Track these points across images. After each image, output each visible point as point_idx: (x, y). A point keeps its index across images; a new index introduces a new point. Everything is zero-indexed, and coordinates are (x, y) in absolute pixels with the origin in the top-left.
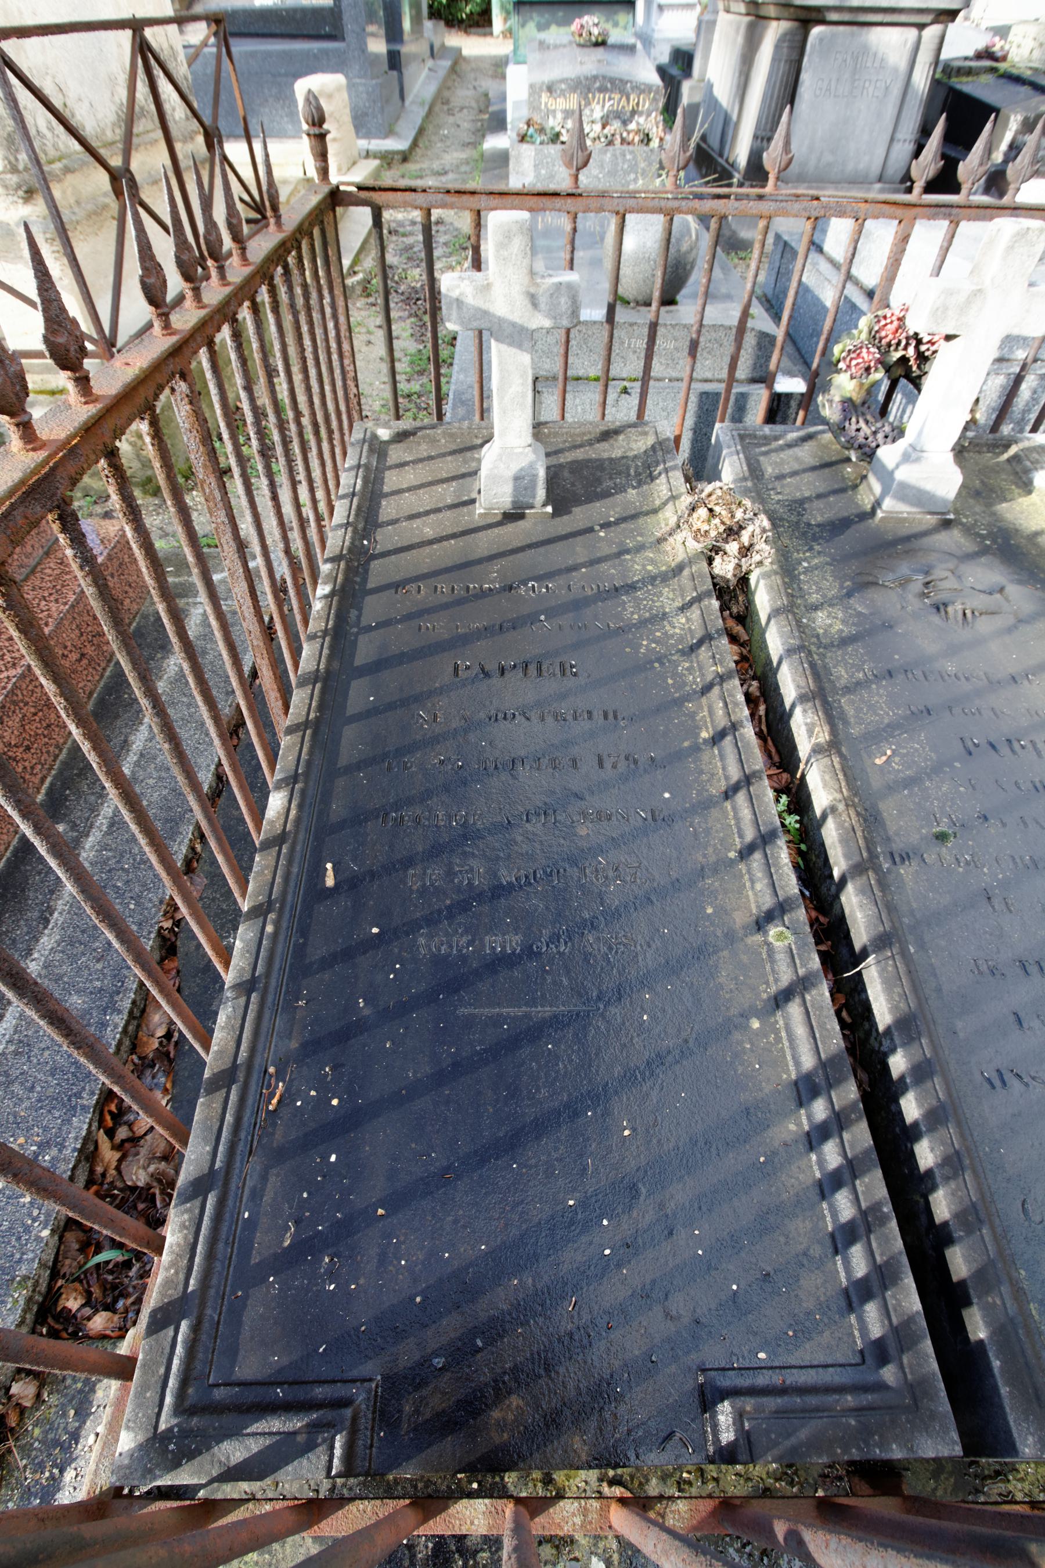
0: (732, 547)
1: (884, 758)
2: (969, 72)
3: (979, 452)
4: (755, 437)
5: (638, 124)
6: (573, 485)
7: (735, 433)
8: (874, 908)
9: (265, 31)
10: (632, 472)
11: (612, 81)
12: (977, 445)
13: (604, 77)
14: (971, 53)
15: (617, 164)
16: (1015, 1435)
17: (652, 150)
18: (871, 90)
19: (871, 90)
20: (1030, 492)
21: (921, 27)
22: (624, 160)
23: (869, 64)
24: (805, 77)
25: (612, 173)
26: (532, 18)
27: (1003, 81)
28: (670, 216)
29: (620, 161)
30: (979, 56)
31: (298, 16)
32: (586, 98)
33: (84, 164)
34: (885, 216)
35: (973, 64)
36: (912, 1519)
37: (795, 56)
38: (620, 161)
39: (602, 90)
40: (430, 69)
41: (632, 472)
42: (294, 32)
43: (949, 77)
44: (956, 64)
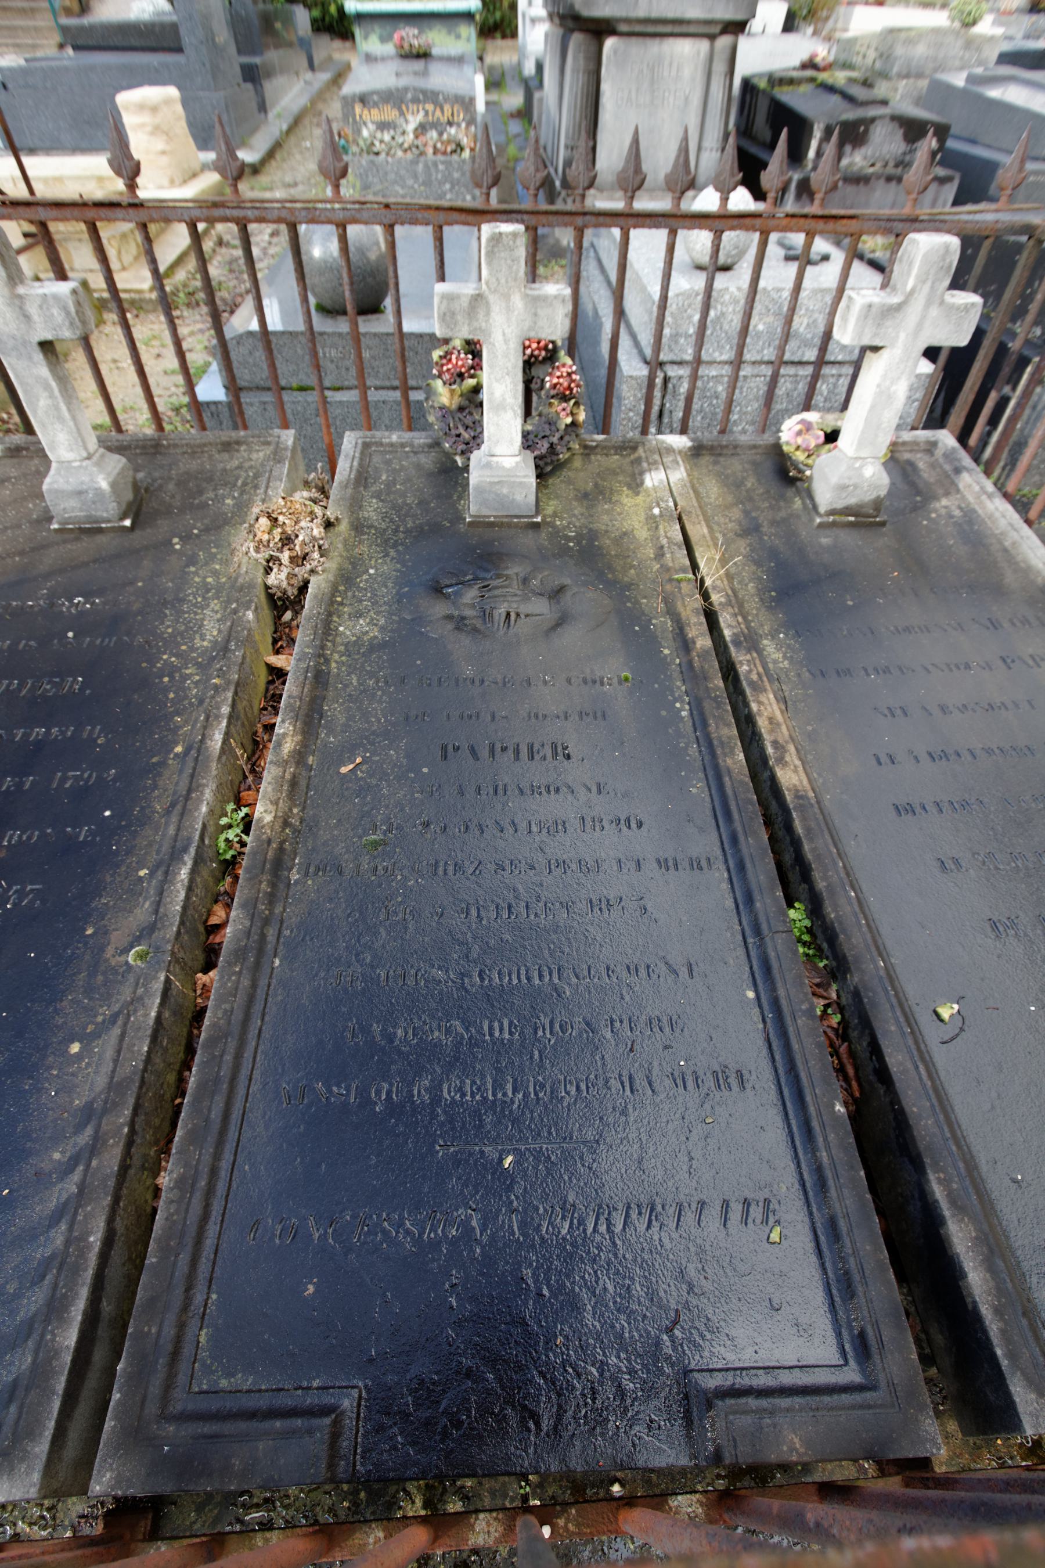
0: (285, 556)
1: (351, 766)
2: (791, 82)
3: (607, 455)
4: (381, 444)
5: (449, 134)
6: (173, 497)
7: (360, 441)
8: (248, 923)
9: (125, 44)
10: (240, 483)
11: (424, 92)
12: (605, 448)
13: (415, 89)
14: (797, 63)
15: (430, 175)
16: (95, 1472)
17: (464, 161)
18: (671, 100)
19: (671, 100)
20: (637, 494)
21: (712, 37)
22: (437, 171)
23: (666, 74)
24: (605, 87)
25: (427, 183)
26: (373, 30)
27: (819, 91)
28: (342, 227)
29: (433, 170)
30: (804, 66)
31: (157, 29)
32: (400, 109)
33: (39, 179)
34: (457, 223)
35: (795, 74)
36: (911, 1492)
37: (592, 66)
38: (433, 170)
39: (416, 101)
40: (306, 82)
41: (240, 483)
42: (154, 45)
43: (773, 87)
44: (777, 75)
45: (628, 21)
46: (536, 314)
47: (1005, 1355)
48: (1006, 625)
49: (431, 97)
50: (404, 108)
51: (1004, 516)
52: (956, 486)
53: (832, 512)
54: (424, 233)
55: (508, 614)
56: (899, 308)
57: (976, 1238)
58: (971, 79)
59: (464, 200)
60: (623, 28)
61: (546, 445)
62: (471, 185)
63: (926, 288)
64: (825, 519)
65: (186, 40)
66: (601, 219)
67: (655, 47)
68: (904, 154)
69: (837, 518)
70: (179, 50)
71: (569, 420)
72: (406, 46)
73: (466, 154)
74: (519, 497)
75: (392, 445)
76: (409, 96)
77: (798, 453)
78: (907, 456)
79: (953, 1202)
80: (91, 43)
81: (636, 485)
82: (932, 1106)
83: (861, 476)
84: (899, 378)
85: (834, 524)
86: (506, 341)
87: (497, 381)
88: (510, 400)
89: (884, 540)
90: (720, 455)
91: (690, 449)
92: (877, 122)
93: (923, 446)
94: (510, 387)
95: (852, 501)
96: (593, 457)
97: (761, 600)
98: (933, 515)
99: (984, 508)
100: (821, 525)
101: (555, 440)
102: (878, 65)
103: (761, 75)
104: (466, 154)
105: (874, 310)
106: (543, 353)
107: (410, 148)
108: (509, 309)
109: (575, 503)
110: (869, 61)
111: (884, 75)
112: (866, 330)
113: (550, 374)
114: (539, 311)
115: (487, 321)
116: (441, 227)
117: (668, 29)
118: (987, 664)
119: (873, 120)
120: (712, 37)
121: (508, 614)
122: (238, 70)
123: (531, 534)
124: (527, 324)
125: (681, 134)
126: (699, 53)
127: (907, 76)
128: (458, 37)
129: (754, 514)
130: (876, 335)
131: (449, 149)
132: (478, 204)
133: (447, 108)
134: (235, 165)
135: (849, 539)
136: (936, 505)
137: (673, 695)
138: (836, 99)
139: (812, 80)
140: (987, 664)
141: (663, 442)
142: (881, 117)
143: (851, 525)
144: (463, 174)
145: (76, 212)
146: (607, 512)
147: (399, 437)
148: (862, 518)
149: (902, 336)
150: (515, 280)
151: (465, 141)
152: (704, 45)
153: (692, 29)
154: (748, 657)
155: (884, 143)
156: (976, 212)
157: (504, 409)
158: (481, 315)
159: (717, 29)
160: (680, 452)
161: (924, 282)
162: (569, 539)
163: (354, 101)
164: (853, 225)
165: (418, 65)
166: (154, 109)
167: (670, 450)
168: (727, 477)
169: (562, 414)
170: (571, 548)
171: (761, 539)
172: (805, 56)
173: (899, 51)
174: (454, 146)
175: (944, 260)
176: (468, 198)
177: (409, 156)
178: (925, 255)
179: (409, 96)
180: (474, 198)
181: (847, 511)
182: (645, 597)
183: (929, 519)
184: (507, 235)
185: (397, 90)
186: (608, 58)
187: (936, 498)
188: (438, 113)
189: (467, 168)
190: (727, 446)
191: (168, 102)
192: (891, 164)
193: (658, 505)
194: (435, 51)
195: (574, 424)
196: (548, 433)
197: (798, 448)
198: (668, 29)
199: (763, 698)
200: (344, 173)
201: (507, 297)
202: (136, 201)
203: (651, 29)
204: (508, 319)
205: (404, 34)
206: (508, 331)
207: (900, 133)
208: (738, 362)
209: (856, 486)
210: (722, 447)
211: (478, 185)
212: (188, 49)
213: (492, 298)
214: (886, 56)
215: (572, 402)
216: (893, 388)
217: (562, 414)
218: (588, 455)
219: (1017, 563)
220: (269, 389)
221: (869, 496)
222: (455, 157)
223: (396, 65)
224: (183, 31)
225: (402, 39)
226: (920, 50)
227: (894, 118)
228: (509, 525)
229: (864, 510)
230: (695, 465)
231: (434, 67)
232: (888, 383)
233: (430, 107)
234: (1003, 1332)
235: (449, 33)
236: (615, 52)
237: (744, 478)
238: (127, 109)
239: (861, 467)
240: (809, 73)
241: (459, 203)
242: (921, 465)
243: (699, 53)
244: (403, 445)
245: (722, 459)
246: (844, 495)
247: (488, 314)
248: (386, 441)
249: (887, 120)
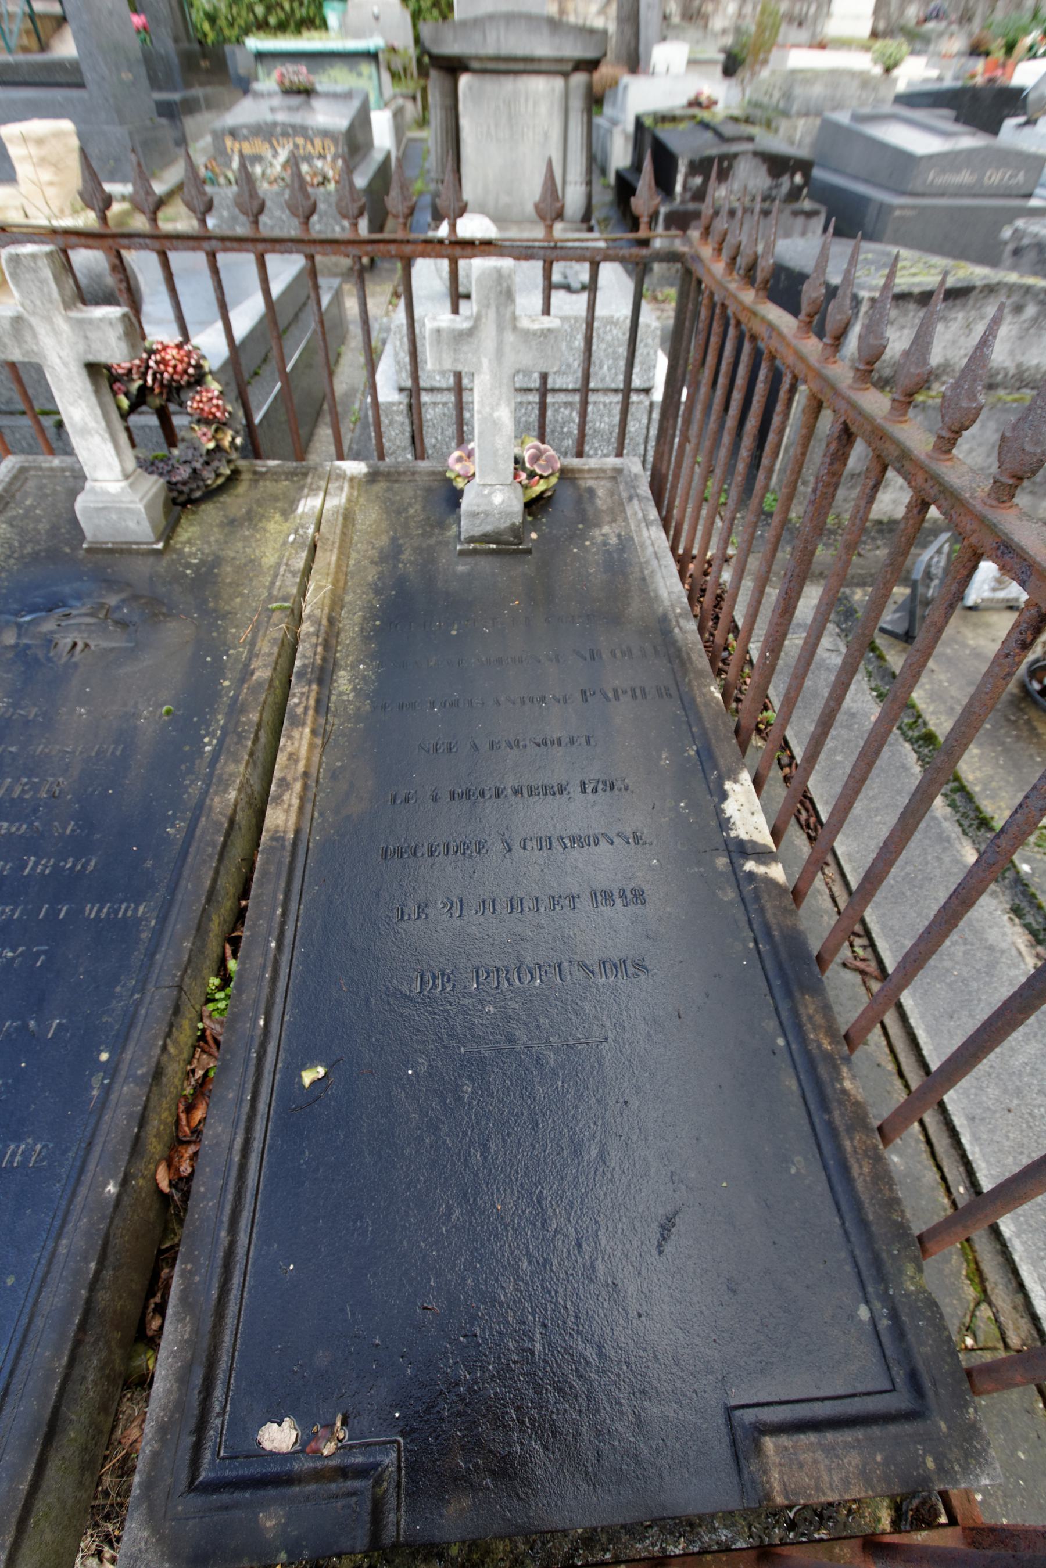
3: (276, 481)
4: (41, 469)
11: (293, 127)
12: (275, 473)
14: (683, 101)
17: (329, 193)
24: (464, 122)
35: (678, 112)
37: (449, 102)
39: (285, 134)
45: (479, 58)
46: (86, 338)
47: (140, 1484)
48: (606, 656)
49: (302, 131)
50: (275, 142)
51: (653, 545)
52: (624, 511)
53: (471, 540)
54: (248, 259)
55: (75, 645)
56: (471, 332)
57: (186, 1341)
58: (857, 118)
59: (333, 231)
60: (475, 65)
61: (189, 470)
62: (338, 217)
63: (492, 314)
64: (466, 546)
65: (88, 76)
66: (228, 244)
67: (509, 84)
68: (771, 188)
69: (478, 546)
70: (81, 85)
71: (211, 445)
72: (287, 83)
73: (331, 187)
74: (132, 525)
75: (52, 469)
76: (279, 130)
77: (459, 480)
78: (591, 483)
79: (184, 1299)
80: (17, 78)
81: (287, 512)
82: (224, 1188)
83: (491, 503)
84: (498, 404)
85: (475, 552)
86: (65, 365)
87: (71, 404)
88: (92, 424)
89: (525, 568)
90: (396, 481)
91: (366, 475)
92: (739, 158)
93: (609, 474)
94: (87, 411)
95: (488, 528)
96: (261, 483)
97: (362, 630)
98: (587, 543)
99: (640, 536)
100: (462, 553)
101: (198, 465)
102: (782, 105)
103: (648, 114)
104: (331, 187)
105: (444, 335)
106: (185, 378)
107: (275, 180)
108: (56, 332)
109: (215, 530)
110: (775, 100)
111: (785, 114)
112: (444, 356)
113: (193, 399)
114: (89, 334)
115: (37, 344)
116: (551, 263)
117: (520, 66)
118: (564, 698)
119: (735, 156)
120: (566, 75)
121: (75, 645)
122: (153, 105)
123: (151, 559)
124: (81, 347)
125: (544, 169)
126: (553, 90)
127: (807, 114)
128: (360, 75)
129: (401, 541)
130: (456, 360)
131: (315, 182)
132: (348, 235)
133: (318, 142)
134: (151, 200)
135: (485, 565)
136: (596, 532)
137: (207, 729)
138: (709, 135)
139: (693, 117)
140: (564, 698)
141: (339, 468)
142: (744, 153)
143: (492, 552)
144: (330, 205)
145: (250, 246)
146: (245, 539)
147: (62, 462)
148: (505, 545)
149: (485, 362)
150: (51, 301)
151: (330, 174)
152: (558, 83)
153: (544, 67)
154: (306, 689)
155: (749, 178)
156: (587, 240)
157: (89, 433)
158: (28, 337)
159: (569, 67)
160: (352, 479)
161: (488, 306)
162: (188, 565)
163: (223, 134)
164: (408, 249)
165: (296, 101)
166: (40, 141)
167: (341, 476)
168: (393, 504)
169: (204, 439)
170: (187, 576)
171: (395, 566)
172: (691, 95)
173: (798, 91)
174: (320, 179)
175: (500, 284)
176: (337, 228)
177: (275, 188)
178: (478, 280)
179: (279, 130)
180: (343, 228)
181: (486, 538)
182: (236, 627)
183: (582, 548)
184: (25, 256)
185: (266, 124)
186: (464, 94)
187: (599, 525)
188: (309, 146)
189: (334, 199)
190: (404, 473)
191: (58, 135)
192: (759, 199)
193: (296, 532)
194: (319, 88)
195: (218, 448)
196: (190, 457)
197: (459, 476)
198: (520, 66)
199: (296, 734)
200: (313, 210)
201: (49, 320)
202: (157, 233)
203: (502, 66)
204: (59, 342)
205: (284, 70)
206: (63, 354)
207: (763, 169)
208: (585, 390)
209: (487, 514)
210: (399, 473)
211: (345, 216)
212: (90, 85)
213: (34, 321)
214: (788, 95)
215: (214, 427)
216: (496, 415)
217: (204, 439)
218: (256, 481)
219: (648, 593)
220: (23, 413)
221: (504, 524)
222: (322, 189)
223: (277, 101)
224: (84, 68)
225: (282, 75)
226: (817, 90)
227: (756, 154)
228: (130, 552)
229: (505, 537)
230: (366, 491)
231: (317, 103)
232: (488, 409)
233: (300, 141)
234: (155, 1454)
235: (351, 70)
236: (470, 88)
237: (410, 505)
238: (11, 141)
239: (490, 494)
240: (696, 111)
241: (329, 235)
242: (600, 492)
243: (553, 90)
244: (63, 470)
245: (396, 486)
246: (478, 522)
247: (35, 336)
248: (45, 465)
249: (750, 156)
